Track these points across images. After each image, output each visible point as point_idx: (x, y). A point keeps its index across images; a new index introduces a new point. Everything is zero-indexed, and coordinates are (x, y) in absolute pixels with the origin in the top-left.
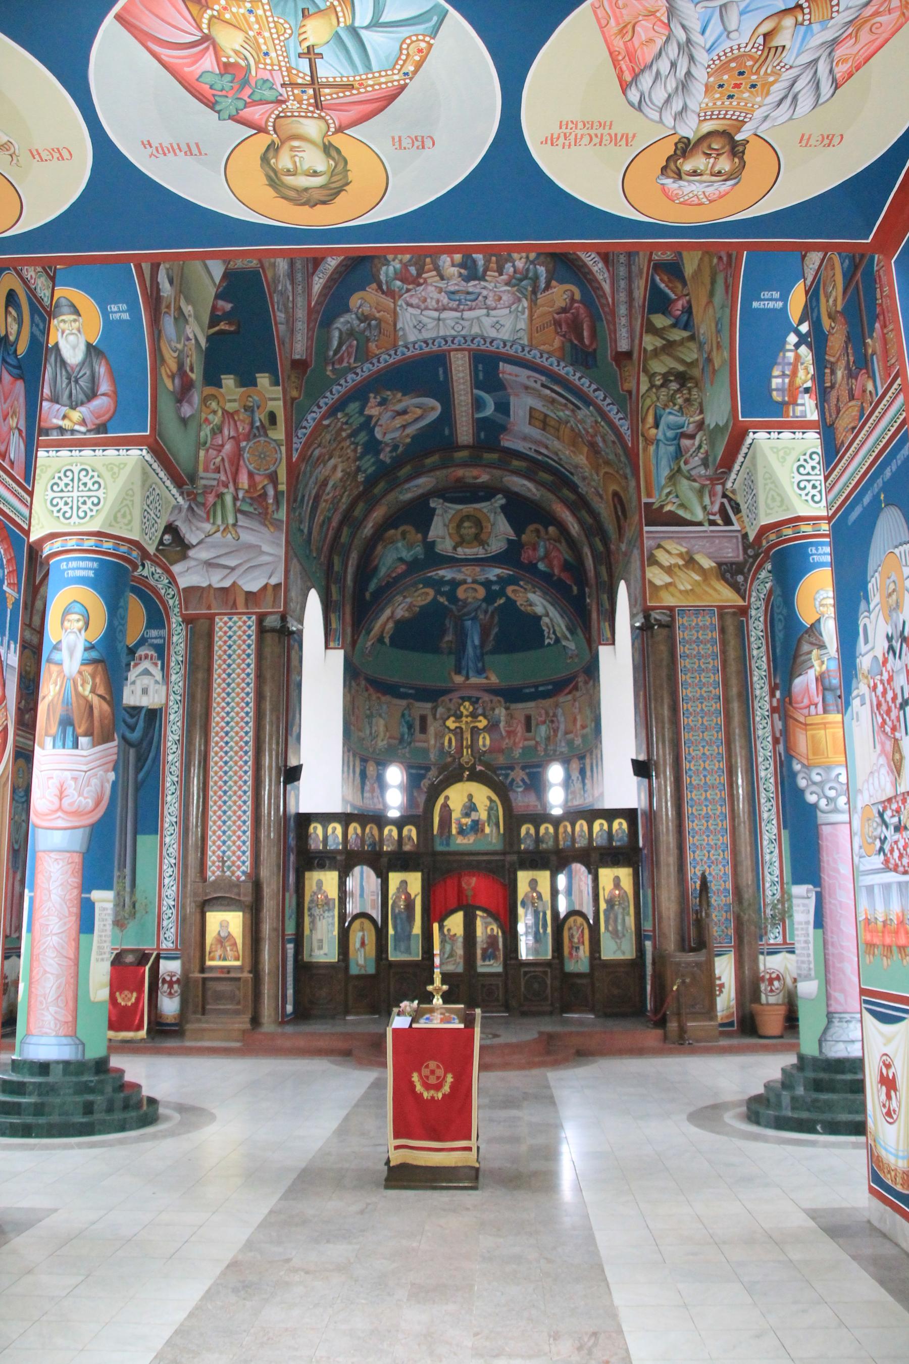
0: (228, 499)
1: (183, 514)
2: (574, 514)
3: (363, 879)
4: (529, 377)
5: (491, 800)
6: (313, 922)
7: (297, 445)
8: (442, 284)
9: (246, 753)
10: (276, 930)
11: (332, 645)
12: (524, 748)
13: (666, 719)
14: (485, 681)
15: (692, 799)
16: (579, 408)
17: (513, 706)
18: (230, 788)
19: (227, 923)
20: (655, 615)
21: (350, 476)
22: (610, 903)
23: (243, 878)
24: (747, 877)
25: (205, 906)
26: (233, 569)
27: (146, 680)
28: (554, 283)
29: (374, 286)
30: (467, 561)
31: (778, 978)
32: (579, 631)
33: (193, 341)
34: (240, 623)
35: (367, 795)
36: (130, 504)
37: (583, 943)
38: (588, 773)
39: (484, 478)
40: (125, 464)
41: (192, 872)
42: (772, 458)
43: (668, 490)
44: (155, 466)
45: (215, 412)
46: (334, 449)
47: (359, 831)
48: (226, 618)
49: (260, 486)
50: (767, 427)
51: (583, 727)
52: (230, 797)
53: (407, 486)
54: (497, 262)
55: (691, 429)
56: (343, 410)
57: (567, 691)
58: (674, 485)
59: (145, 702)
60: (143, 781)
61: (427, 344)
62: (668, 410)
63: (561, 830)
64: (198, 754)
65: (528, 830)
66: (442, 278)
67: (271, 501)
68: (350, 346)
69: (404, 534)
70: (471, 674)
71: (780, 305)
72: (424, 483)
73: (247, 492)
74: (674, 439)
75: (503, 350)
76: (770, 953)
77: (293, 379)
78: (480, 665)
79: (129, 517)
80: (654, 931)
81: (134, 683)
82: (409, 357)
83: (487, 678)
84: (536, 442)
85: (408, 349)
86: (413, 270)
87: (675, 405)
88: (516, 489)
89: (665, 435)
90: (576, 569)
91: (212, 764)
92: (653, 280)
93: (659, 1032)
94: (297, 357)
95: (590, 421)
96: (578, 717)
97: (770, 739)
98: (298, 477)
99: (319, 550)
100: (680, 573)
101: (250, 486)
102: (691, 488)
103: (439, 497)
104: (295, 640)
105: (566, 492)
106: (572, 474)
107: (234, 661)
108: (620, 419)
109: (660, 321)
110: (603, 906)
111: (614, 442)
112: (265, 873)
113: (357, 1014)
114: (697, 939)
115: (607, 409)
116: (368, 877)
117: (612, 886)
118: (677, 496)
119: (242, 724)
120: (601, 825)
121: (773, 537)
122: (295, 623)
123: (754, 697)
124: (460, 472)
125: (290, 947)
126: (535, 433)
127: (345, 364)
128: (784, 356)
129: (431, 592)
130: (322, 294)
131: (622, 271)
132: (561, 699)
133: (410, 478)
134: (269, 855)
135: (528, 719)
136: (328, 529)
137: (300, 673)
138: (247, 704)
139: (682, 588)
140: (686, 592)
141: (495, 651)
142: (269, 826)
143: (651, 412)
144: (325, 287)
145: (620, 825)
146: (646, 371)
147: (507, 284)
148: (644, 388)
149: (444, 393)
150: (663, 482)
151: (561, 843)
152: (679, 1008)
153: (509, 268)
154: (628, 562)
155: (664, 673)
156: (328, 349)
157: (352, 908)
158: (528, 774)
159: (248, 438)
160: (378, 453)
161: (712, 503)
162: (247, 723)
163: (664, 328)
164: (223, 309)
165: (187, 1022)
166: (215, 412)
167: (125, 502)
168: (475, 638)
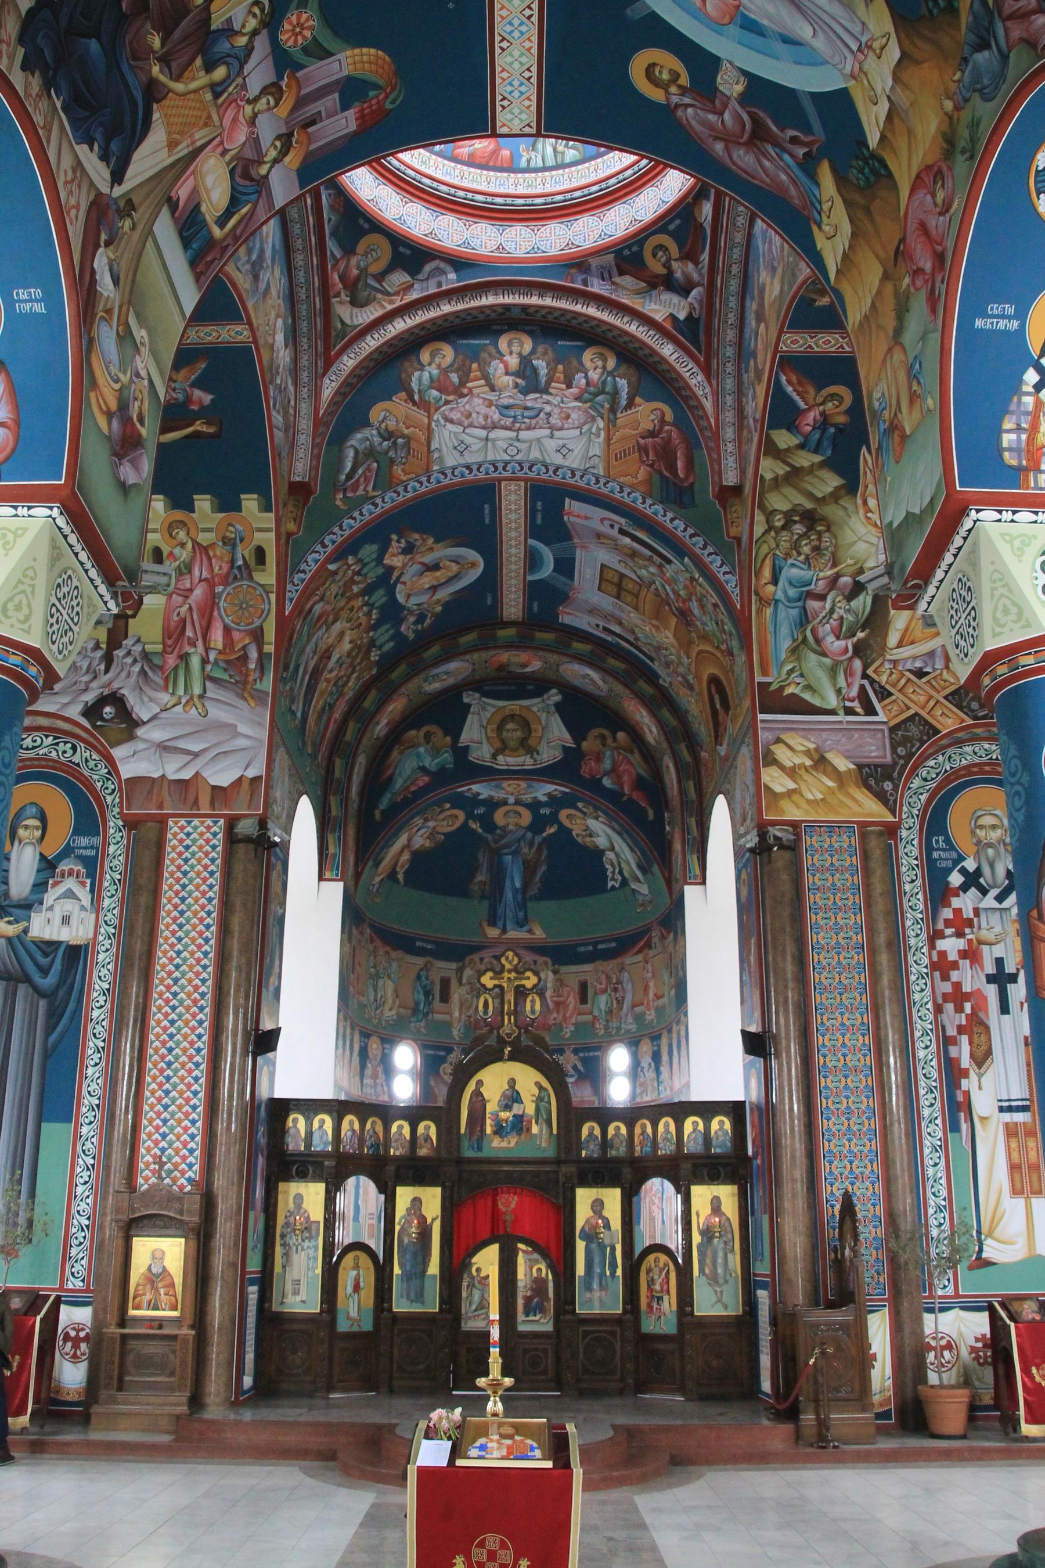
0: (195, 662)
1: (133, 679)
2: (653, 714)
3: (360, 1195)
4: (602, 520)
5: (540, 1087)
6: (286, 1255)
7: (293, 593)
8: (492, 396)
9: (202, 1009)
10: (234, 1265)
11: (328, 875)
12: (576, 1025)
13: (789, 976)
15: (826, 1087)
17: (564, 969)
18: (177, 1058)
19: (161, 1254)
21: (362, 650)
22: (707, 1233)
23: (189, 1188)
24: (905, 1203)
25: (132, 1227)
26: (196, 755)
27: (68, 905)
28: (638, 400)
29: (403, 395)
31: (949, 1347)
32: (655, 868)
33: (146, 382)
34: (202, 829)
35: (367, 1081)
36: (29, 590)
37: (668, 1292)
38: (665, 1058)
39: (536, 665)
40: (25, 530)
41: (117, 1180)
42: (1004, 550)
43: (790, 667)
44: (73, 539)
45: (183, 545)
47: (357, 1126)
48: (183, 822)
49: (240, 646)
50: (997, 502)
51: (658, 997)
52: (176, 1071)
54: (565, 372)
55: (820, 587)
56: (355, 553)
58: (798, 659)
59: (65, 935)
60: (55, 1047)
61: (471, 471)
62: (790, 561)
63: (638, 1130)
64: (134, 1013)
65: (592, 1129)
66: (493, 389)
67: (252, 666)
68: (369, 469)
69: (428, 736)
70: (509, 926)
71: (1015, 325)
72: (456, 669)
73: (220, 652)
75: (572, 481)
76: (942, 1310)
77: (290, 508)
78: (521, 914)
79: (26, 611)
80: (773, 1275)
81: (51, 908)
82: (445, 487)
83: (530, 931)
84: (607, 616)
85: (446, 475)
86: (454, 378)
87: (799, 554)
88: (576, 682)
89: (785, 592)
90: (652, 786)
91: (153, 1023)
92: (778, 381)
93: (787, 1428)
94: (298, 479)
95: (683, 578)
96: (651, 984)
97: (930, 1006)
98: (291, 638)
99: (317, 748)
100: (806, 776)
102: (821, 665)
103: (475, 690)
104: (278, 858)
105: (642, 685)
106: (652, 659)
107: (191, 881)
108: (725, 573)
109: (784, 439)
110: (696, 1238)
111: (715, 605)
112: (220, 1182)
113: (345, 1390)
114: (840, 1290)
115: (707, 560)
116: (366, 1193)
117: (709, 1211)
118: (802, 675)
119: (198, 968)
120: (695, 1123)
121: (1002, 670)
122: (279, 832)
123: (907, 947)
124: (505, 656)
125: (253, 1290)
126: (606, 602)
127: (360, 492)
128: (1019, 402)
129: (461, 815)
130: (333, 402)
131: (730, 384)
132: (628, 960)
133: (437, 662)
134: (228, 1157)
135: (584, 987)
136: (329, 720)
137: (283, 904)
139: (811, 797)
141: (542, 896)
142: (230, 1114)
143: (768, 562)
144: (337, 393)
145: (721, 1125)
146: (762, 507)
147: (578, 399)
148: (759, 530)
149: (487, 541)
150: (783, 656)
151: (638, 1149)
152: (816, 1392)
153: (580, 380)
155: (786, 913)
157: (343, 1236)
158: (583, 1060)
159: (225, 581)
160: (400, 621)
161: (849, 685)
162: (205, 967)
163: (788, 450)
164: (200, 401)
165: (96, 1402)
167: (21, 587)
168: (516, 879)
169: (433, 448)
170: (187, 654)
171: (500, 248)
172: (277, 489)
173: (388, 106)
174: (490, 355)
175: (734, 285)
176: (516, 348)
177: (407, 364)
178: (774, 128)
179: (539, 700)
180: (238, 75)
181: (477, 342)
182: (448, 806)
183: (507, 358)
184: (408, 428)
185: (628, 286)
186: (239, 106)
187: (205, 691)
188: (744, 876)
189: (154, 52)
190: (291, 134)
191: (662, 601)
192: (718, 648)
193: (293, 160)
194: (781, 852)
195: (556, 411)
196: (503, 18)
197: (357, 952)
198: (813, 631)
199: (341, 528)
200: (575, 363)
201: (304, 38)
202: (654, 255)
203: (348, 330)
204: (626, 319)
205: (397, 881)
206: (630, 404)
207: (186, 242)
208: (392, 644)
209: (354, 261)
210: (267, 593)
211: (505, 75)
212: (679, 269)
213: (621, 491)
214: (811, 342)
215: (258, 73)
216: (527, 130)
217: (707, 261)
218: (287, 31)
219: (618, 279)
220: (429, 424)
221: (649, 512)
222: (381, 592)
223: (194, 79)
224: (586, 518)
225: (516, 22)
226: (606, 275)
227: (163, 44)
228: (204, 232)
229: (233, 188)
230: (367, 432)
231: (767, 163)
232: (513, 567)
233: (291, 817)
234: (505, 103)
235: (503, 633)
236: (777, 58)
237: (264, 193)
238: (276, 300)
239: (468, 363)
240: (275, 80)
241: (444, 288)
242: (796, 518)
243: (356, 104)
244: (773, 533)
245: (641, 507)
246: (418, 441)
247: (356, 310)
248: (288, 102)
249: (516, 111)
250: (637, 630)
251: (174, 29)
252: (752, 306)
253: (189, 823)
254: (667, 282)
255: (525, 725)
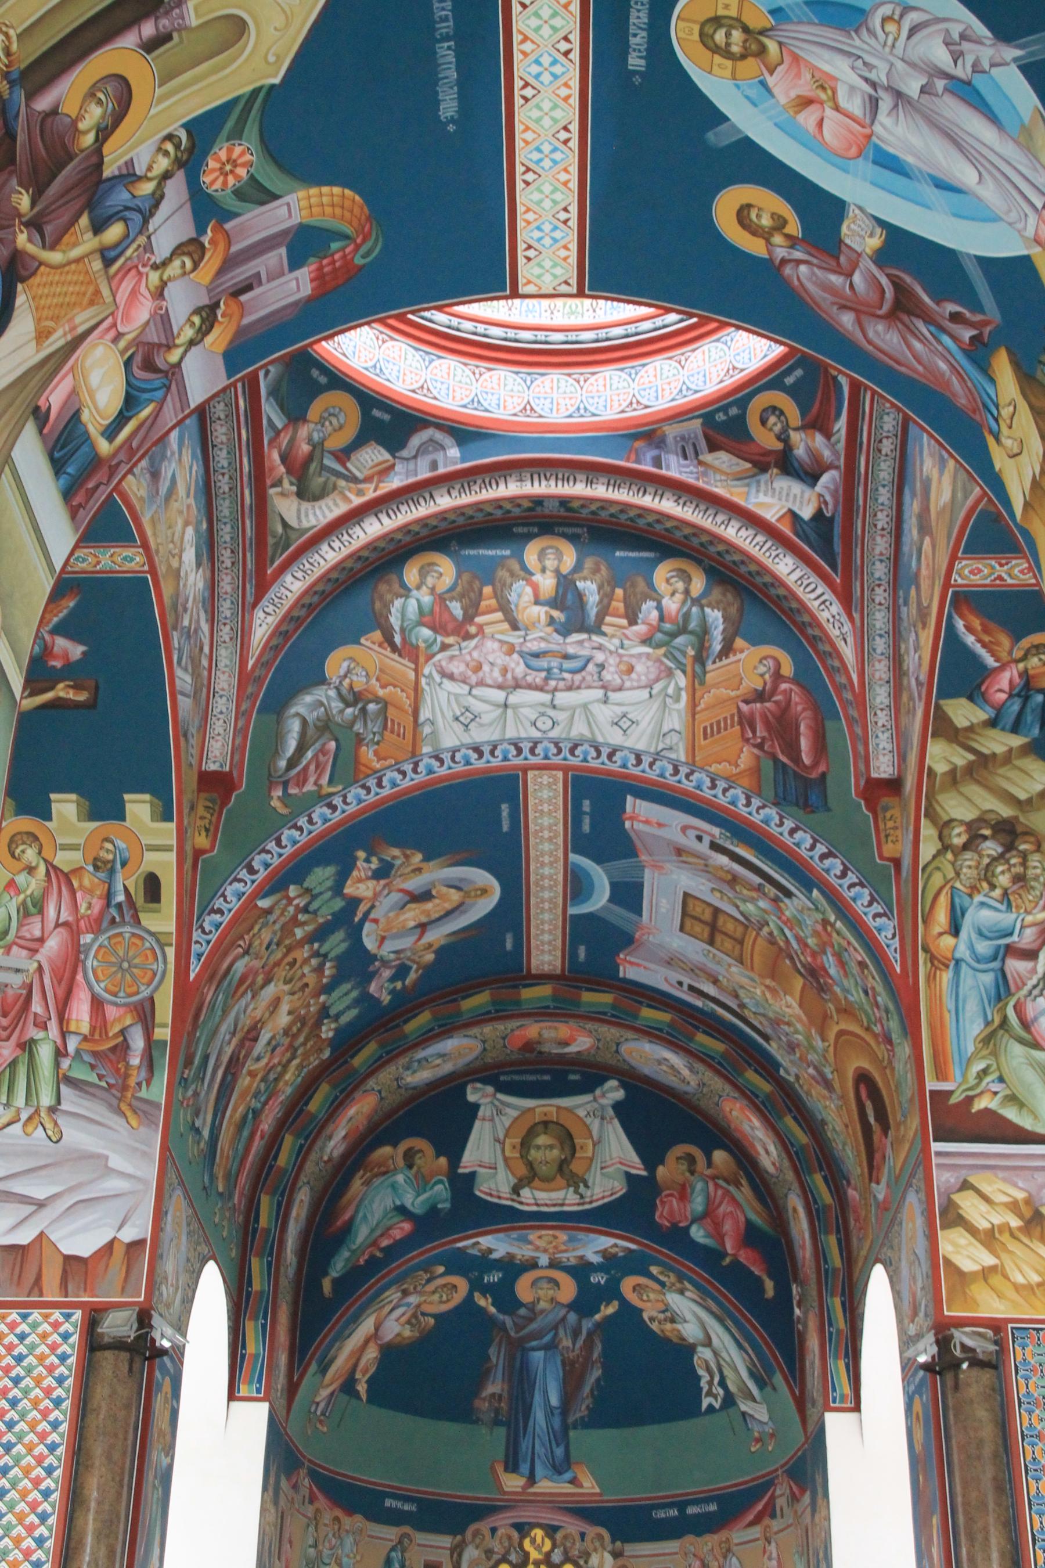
0: (45, 1053)
4: (684, 829)
7: (201, 945)
8: (515, 638)
11: (243, 1390)
14: (569, 1489)
16: (789, 894)
17: (630, 1549)
20: (962, 1337)
21: (307, 1024)
26: (41, 1205)
28: (739, 642)
29: (377, 635)
30: (540, 1219)
32: (778, 1379)
34: (46, 1327)
39: (582, 1043)
45: (31, 870)
46: (278, 964)
49: (116, 1029)
53: (421, 1054)
54: (626, 600)
55: (1027, 938)
56: (299, 882)
57: (750, 1517)
58: (995, 1054)
61: (481, 754)
62: (978, 898)
66: (515, 626)
67: (135, 1061)
68: (323, 751)
69: (409, 1157)
70: (539, 1471)
72: (456, 1050)
73: (85, 1038)
74: (994, 958)
75: (636, 771)
77: (201, 811)
78: (559, 1452)
82: (441, 779)
83: (574, 1481)
84: (695, 970)
85: (442, 762)
86: (456, 609)
87: (993, 887)
88: (646, 1070)
89: (972, 947)
90: (771, 1243)
94: (213, 767)
95: (811, 921)
98: (197, 1016)
99: (232, 1179)
100: (1012, 1245)
101: (93, 1029)
103: (485, 1081)
104: (165, 1371)
106: (767, 1038)
108: (876, 916)
109: (963, 712)
111: (862, 965)
115: (848, 894)
118: (1001, 1080)
122: (169, 1331)
124: (532, 1030)
126: (693, 949)
127: (309, 787)
129: (462, 1285)
130: (271, 647)
131: (880, 619)
132: (738, 1535)
133: (427, 1038)
137: (170, 1449)
138: (43, 1518)
139: (1020, 1279)
140: (1027, 1290)
141: (596, 1420)
143: (943, 901)
146: (931, 815)
147: (646, 641)
148: (928, 850)
149: (508, 860)
150: (971, 1048)
153: (649, 611)
154: (894, 1221)
155: (988, 1473)
156: (276, 753)
159: (96, 926)
160: (369, 977)
163: (971, 729)
164: (66, 655)
166: (31, 870)
169: (422, 718)
170: (33, 1042)
171: (528, 408)
172: (182, 782)
173: (358, 261)
174: (512, 574)
175: (885, 471)
176: (550, 563)
177: (383, 587)
178: (926, 299)
179: (587, 1098)
180: (140, 232)
181: (490, 553)
182: (441, 1269)
183: (538, 578)
184: (383, 687)
185: (724, 467)
186: (140, 274)
187: (59, 1101)
188: (917, 1407)
189: (20, 215)
190: (217, 305)
191: (779, 952)
192: (868, 1029)
193: (218, 339)
194: (976, 1372)
195: (612, 660)
196: (527, 143)
197: (288, 1521)
198: (1018, 1009)
199: (279, 843)
200: (641, 585)
201: (237, 177)
202: (763, 422)
203: (293, 535)
204: (720, 518)
205: (357, 1395)
206: (727, 649)
207: (58, 466)
208: (354, 1012)
209: (303, 431)
210: (162, 946)
211: (530, 216)
212: (802, 444)
213: (714, 786)
214: (1002, 571)
215: (170, 227)
216: (564, 289)
217: (843, 432)
218: (213, 170)
219: (708, 457)
220: (417, 682)
221: (756, 819)
222: (340, 935)
223: (75, 244)
224: (660, 825)
225: (546, 148)
226: (690, 451)
227: (33, 203)
228: (85, 449)
229: (128, 383)
230: (320, 693)
231: (917, 345)
232: (546, 895)
233: (188, 1301)
234: (531, 253)
235: (530, 994)
236: (928, 208)
237: (174, 387)
238: (186, 500)
239: (477, 585)
240: (194, 235)
241: (441, 470)
242: (987, 832)
243: (312, 260)
244: (949, 856)
245: (743, 811)
246: (400, 708)
247: (305, 505)
248: (212, 262)
249: (548, 264)
250: (742, 993)
251: (49, 184)
252: (912, 507)
253: (24, 1317)
254: (785, 463)
255: (567, 1140)
